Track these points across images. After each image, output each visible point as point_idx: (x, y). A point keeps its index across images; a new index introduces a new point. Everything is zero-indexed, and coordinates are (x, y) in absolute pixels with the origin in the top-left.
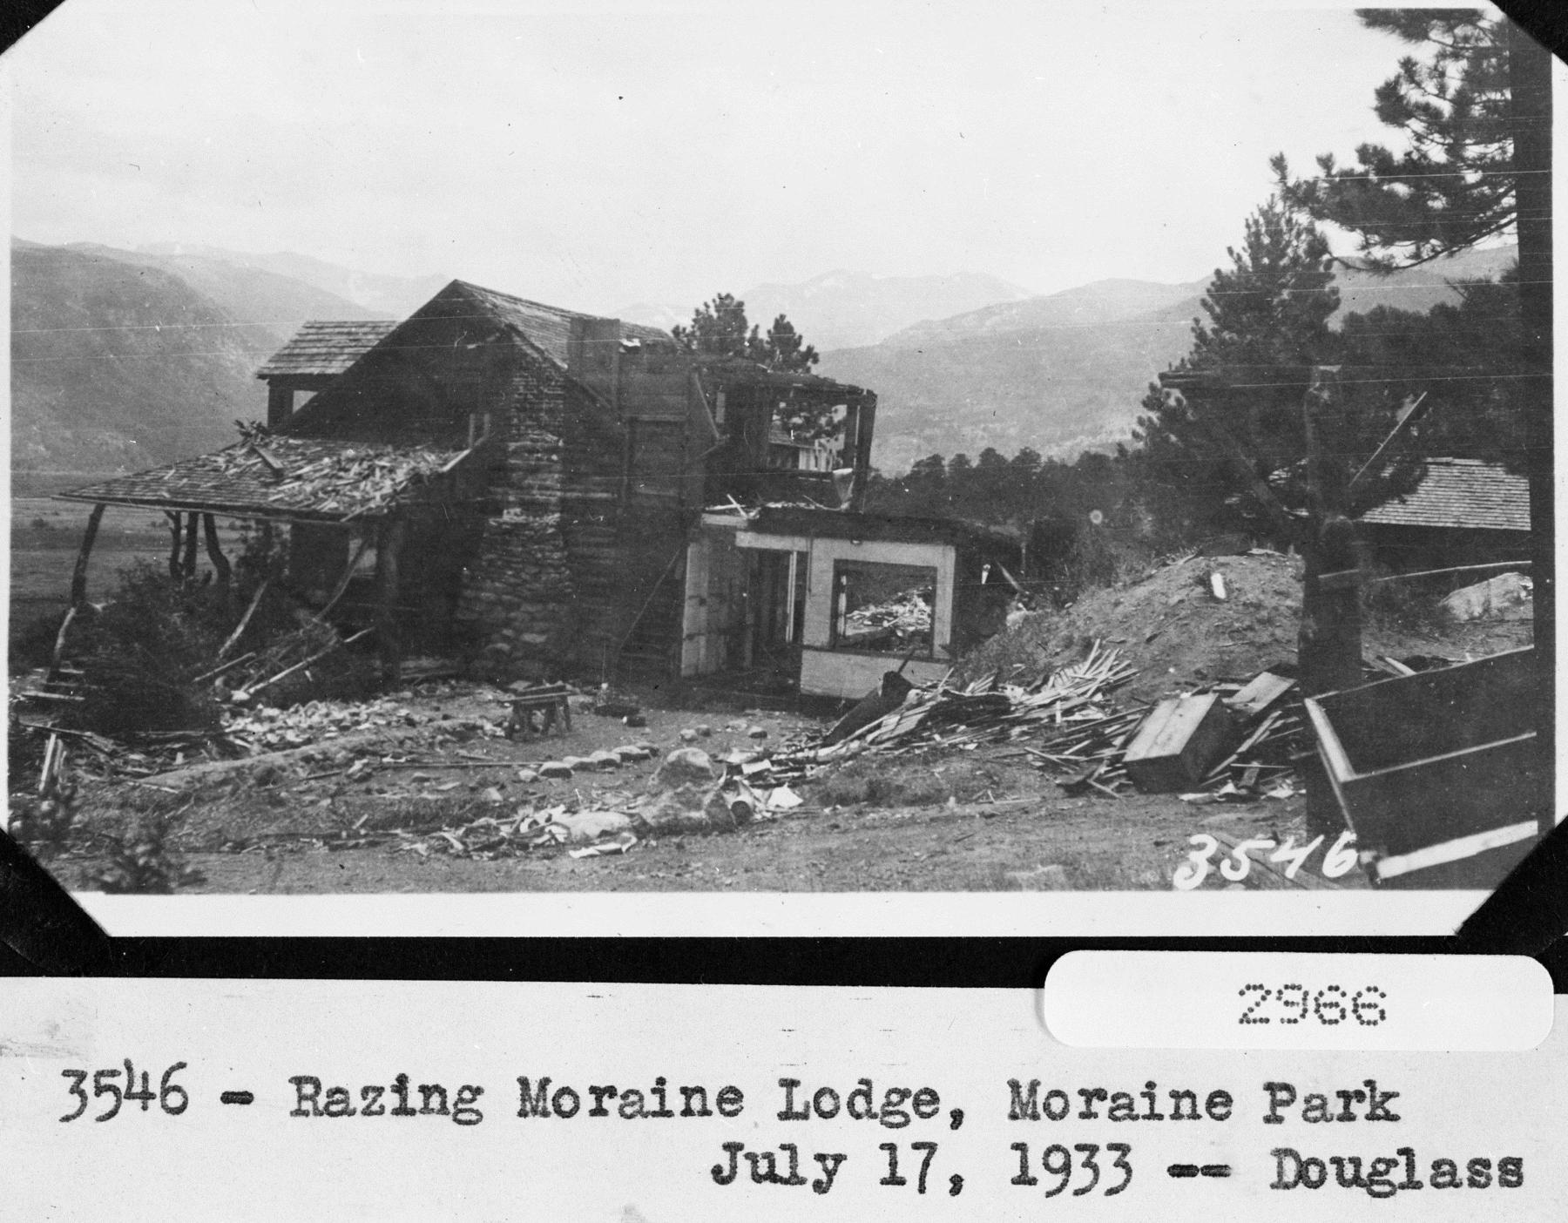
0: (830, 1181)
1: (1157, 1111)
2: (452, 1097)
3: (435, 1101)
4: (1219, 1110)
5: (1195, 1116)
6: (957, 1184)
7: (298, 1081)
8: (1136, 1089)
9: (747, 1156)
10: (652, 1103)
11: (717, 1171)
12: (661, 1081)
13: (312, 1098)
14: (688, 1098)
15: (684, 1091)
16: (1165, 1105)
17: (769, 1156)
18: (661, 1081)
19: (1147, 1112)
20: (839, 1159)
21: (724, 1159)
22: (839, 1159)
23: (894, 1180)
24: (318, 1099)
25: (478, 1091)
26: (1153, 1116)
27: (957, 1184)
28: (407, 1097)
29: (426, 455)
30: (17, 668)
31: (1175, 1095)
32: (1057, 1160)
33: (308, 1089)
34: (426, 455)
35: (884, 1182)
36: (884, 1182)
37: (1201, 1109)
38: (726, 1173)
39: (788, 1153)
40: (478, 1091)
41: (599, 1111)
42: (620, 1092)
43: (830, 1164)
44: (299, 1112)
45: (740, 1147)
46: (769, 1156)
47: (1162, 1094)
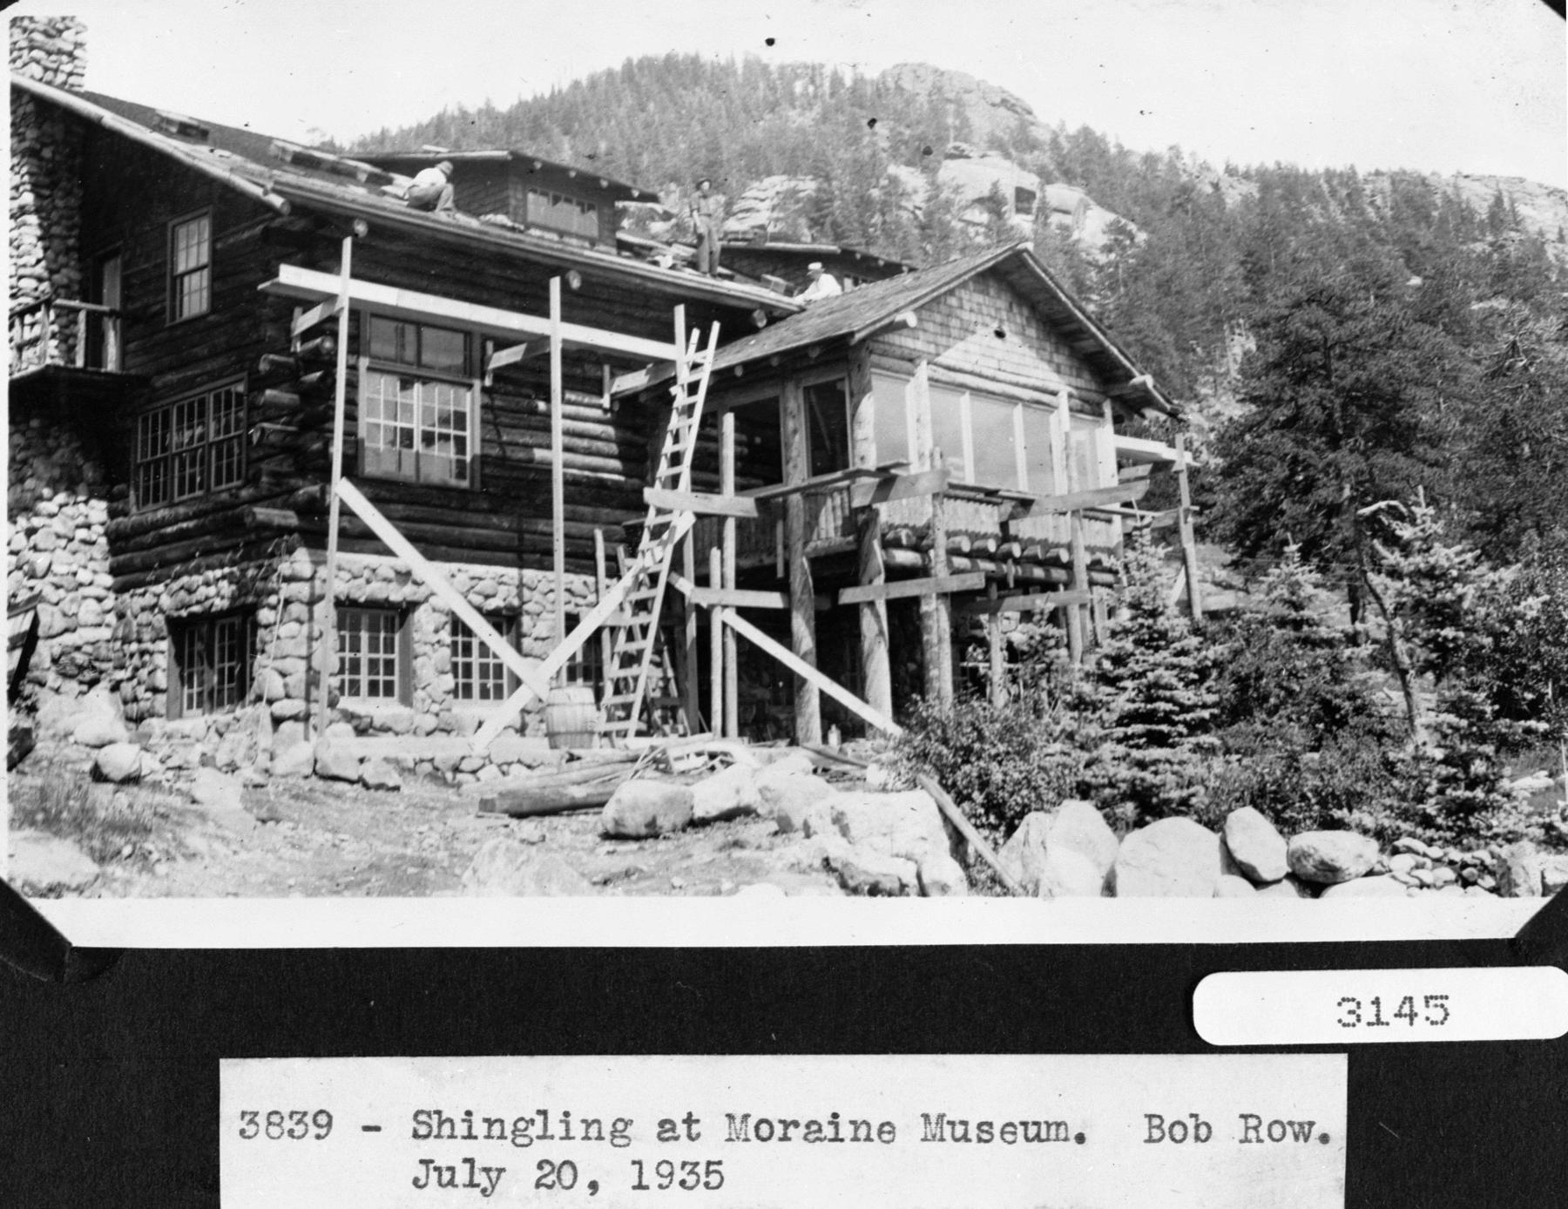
0: (493, 1187)
1: (549, 1133)
2: (509, 1129)
3: (496, 1129)
4: (886, 1137)
5: (868, 1139)
6: (594, 1186)
7: (1150, 1117)
8: (824, 1119)
9: (436, 1169)
10: (828, 1131)
11: (416, 1182)
12: (567, 1114)
13: (1256, 1128)
14: (856, 1129)
15: (486, 1120)
16: (846, 1131)
17: (451, 1169)
18: (835, 1116)
19: (563, 1134)
20: (501, 1171)
21: (420, 1171)
22: (501, 1171)
23: (640, 1186)
24: (938, 1127)
25: (628, 1123)
26: (837, 1139)
27: (594, 1186)
28: (1038, 1132)
29: (284, 568)
30: (1147, 823)
31: (588, 1124)
32: (665, 1169)
33: (1252, 1122)
34: (284, 568)
35: (634, 1188)
36: (634, 1188)
37: (874, 1135)
38: (422, 1182)
39: (468, 1166)
40: (628, 1123)
41: (785, 1138)
42: (803, 1122)
43: (494, 1175)
44: (1150, 1140)
45: (432, 1161)
46: (451, 1169)
47: (843, 1121)
